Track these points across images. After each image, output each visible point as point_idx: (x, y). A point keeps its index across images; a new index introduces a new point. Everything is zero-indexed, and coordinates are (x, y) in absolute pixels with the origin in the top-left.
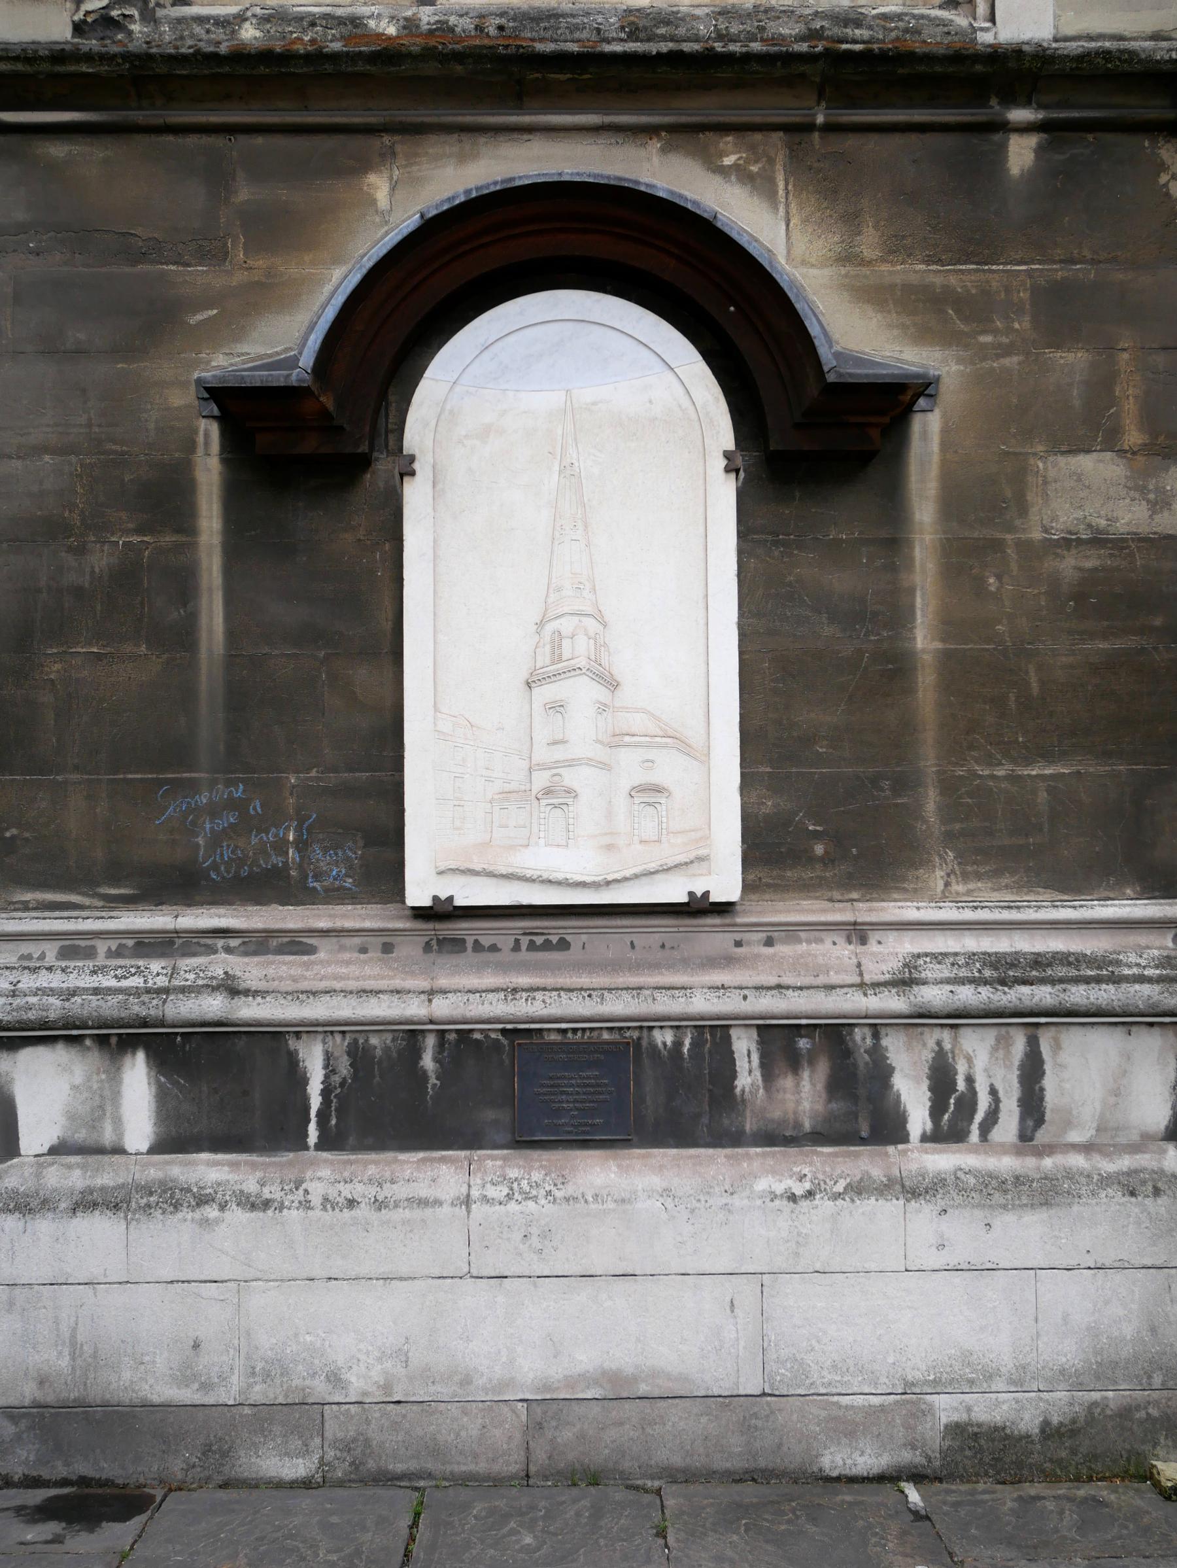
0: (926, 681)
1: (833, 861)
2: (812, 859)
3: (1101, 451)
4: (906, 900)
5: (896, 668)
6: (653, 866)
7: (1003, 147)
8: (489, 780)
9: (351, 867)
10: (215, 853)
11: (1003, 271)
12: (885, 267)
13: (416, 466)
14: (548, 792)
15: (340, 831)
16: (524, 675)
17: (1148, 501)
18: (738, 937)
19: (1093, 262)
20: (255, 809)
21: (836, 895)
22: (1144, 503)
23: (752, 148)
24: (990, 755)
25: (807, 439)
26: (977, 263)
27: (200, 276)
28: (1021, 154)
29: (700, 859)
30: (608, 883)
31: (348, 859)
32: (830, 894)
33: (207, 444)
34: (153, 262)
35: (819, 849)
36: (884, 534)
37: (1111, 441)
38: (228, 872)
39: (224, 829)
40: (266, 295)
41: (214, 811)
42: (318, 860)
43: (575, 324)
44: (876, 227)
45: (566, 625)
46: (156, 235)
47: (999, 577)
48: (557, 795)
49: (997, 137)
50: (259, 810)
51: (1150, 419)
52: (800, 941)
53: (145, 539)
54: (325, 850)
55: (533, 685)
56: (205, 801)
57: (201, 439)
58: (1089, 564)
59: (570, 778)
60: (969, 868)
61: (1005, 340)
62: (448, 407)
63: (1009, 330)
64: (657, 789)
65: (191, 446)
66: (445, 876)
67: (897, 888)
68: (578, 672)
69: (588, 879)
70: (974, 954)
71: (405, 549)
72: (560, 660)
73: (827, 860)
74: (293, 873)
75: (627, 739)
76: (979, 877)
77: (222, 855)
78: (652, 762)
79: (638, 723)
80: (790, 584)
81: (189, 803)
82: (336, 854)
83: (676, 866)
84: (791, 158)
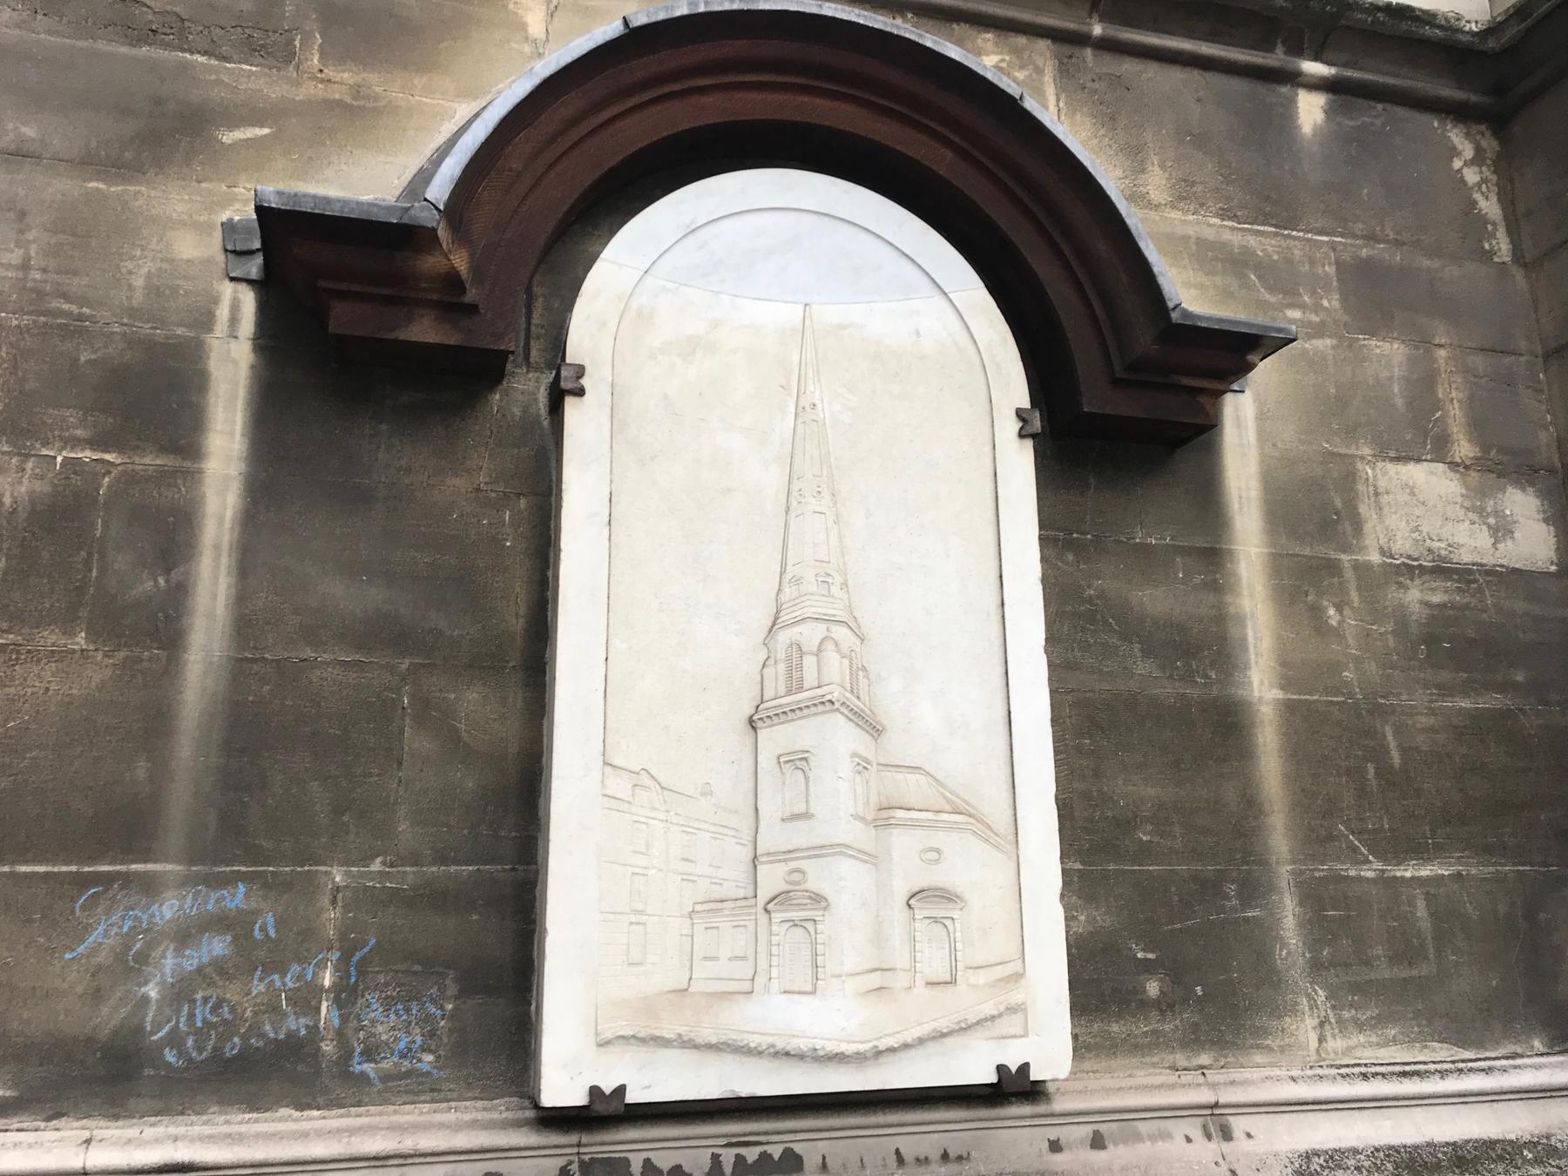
0: (1268, 740)
1: (1171, 1006)
2: (1145, 1004)
3: (1431, 461)
4: (1272, 1065)
5: (1227, 724)
6: (944, 1024)
7: (1292, 102)
8: (688, 879)
9: (432, 1034)
10: (178, 1011)
11: (1308, 240)
12: (1176, 215)
13: (586, 382)
14: (781, 898)
15: (417, 968)
16: (748, 710)
17: (1489, 527)
18: (1053, 1134)
19: (1398, 243)
20: (263, 929)
21: (1180, 1059)
22: (1484, 527)
23: (1016, 51)
24: (1355, 850)
25: (1117, 401)
26: (1275, 226)
27: (247, 77)
28: (1310, 110)
29: (1012, 1010)
30: (878, 1053)
31: (429, 1018)
32: (1171, 1057)
33: (234, 320)
34: (166, 46)
35: (1153, 988)
36: (1200, 542)
37: (1439, 450)
38: (200, 1050)
39: (199, 970)
40: (353, 118)
41: (185, 935)
42: (373, 1022)
43: (815, 217)
44: (1162, 167)
45: (810, 635)
46: (178, 9)
47: (1339, 609)
48: (798, 903)
49: (1285, 90)
50: (272, 933)
51: (1478, 427)
52: (1138, 1138)
53: (108, 457)
54: (388, 1003)
55: (760, 724)
56: (168, 916)
57: (223, 313)
58: (1437, 598)
59: (817, 877)
60: (1346, 1015)
61: (1315, 319)
62: (635, 304)
63: (1317, 308)
64: (946, 896)
65: (205, 320)
66: (611, 1048)
67: (1258, 1047)
68: (828, 706)
69: (849, 1048)
70: (1377, 1150)
71: (565, 504)
72: (801, 689)
73: (1164, 1006)
74: (328, 1047)
75: (900, 814)
76: (1360, 1026)
77: (192, 1016)
78: (938, 851)
79: (912, 787)
80: (1090, 600)
81: (136, 918)
82: (408, 1010)
83: (978, 1023)
84: (1060, 71)
